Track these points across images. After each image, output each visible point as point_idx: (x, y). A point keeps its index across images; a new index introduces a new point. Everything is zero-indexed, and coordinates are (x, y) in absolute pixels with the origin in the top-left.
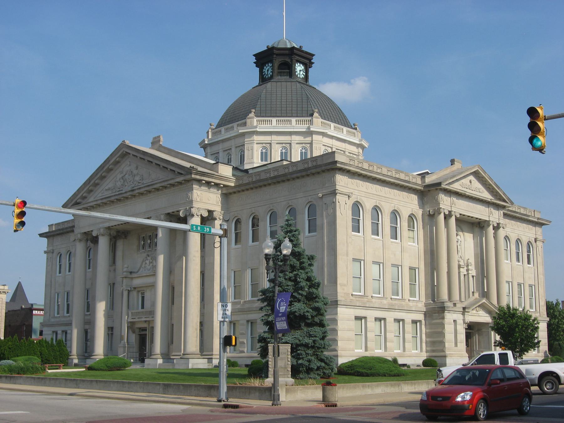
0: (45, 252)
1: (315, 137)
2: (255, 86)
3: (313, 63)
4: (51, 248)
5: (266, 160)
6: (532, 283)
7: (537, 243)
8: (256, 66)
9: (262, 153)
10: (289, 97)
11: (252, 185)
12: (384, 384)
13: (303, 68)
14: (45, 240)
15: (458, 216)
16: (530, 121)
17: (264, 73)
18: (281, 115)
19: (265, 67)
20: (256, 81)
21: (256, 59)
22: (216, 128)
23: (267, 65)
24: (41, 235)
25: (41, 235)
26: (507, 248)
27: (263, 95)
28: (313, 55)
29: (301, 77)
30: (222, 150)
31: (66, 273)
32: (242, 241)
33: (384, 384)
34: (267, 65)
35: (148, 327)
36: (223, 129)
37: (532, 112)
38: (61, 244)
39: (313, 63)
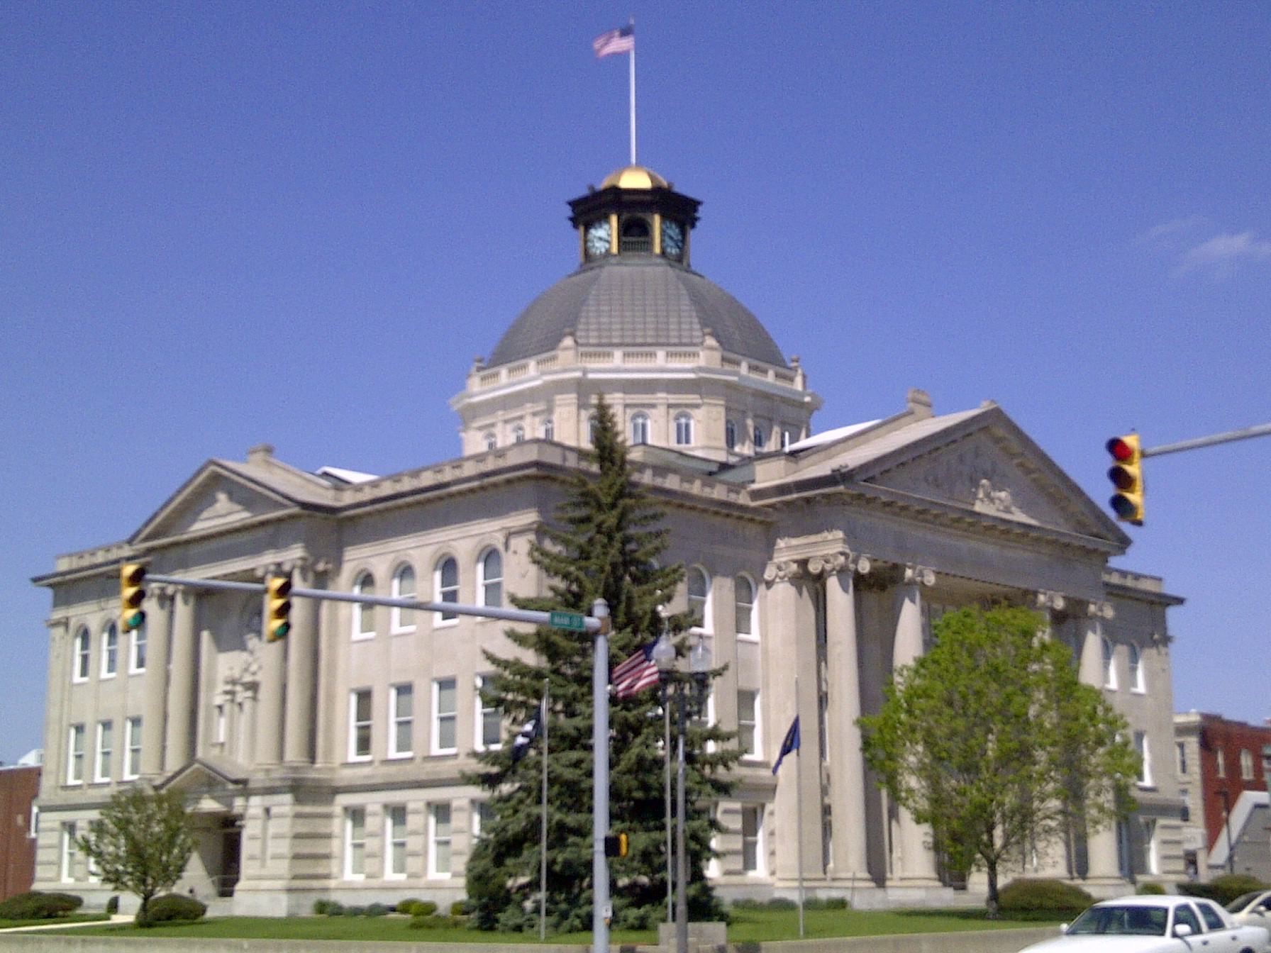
13: (677, 230)
25: (1180, 601)
28: (699, 203)
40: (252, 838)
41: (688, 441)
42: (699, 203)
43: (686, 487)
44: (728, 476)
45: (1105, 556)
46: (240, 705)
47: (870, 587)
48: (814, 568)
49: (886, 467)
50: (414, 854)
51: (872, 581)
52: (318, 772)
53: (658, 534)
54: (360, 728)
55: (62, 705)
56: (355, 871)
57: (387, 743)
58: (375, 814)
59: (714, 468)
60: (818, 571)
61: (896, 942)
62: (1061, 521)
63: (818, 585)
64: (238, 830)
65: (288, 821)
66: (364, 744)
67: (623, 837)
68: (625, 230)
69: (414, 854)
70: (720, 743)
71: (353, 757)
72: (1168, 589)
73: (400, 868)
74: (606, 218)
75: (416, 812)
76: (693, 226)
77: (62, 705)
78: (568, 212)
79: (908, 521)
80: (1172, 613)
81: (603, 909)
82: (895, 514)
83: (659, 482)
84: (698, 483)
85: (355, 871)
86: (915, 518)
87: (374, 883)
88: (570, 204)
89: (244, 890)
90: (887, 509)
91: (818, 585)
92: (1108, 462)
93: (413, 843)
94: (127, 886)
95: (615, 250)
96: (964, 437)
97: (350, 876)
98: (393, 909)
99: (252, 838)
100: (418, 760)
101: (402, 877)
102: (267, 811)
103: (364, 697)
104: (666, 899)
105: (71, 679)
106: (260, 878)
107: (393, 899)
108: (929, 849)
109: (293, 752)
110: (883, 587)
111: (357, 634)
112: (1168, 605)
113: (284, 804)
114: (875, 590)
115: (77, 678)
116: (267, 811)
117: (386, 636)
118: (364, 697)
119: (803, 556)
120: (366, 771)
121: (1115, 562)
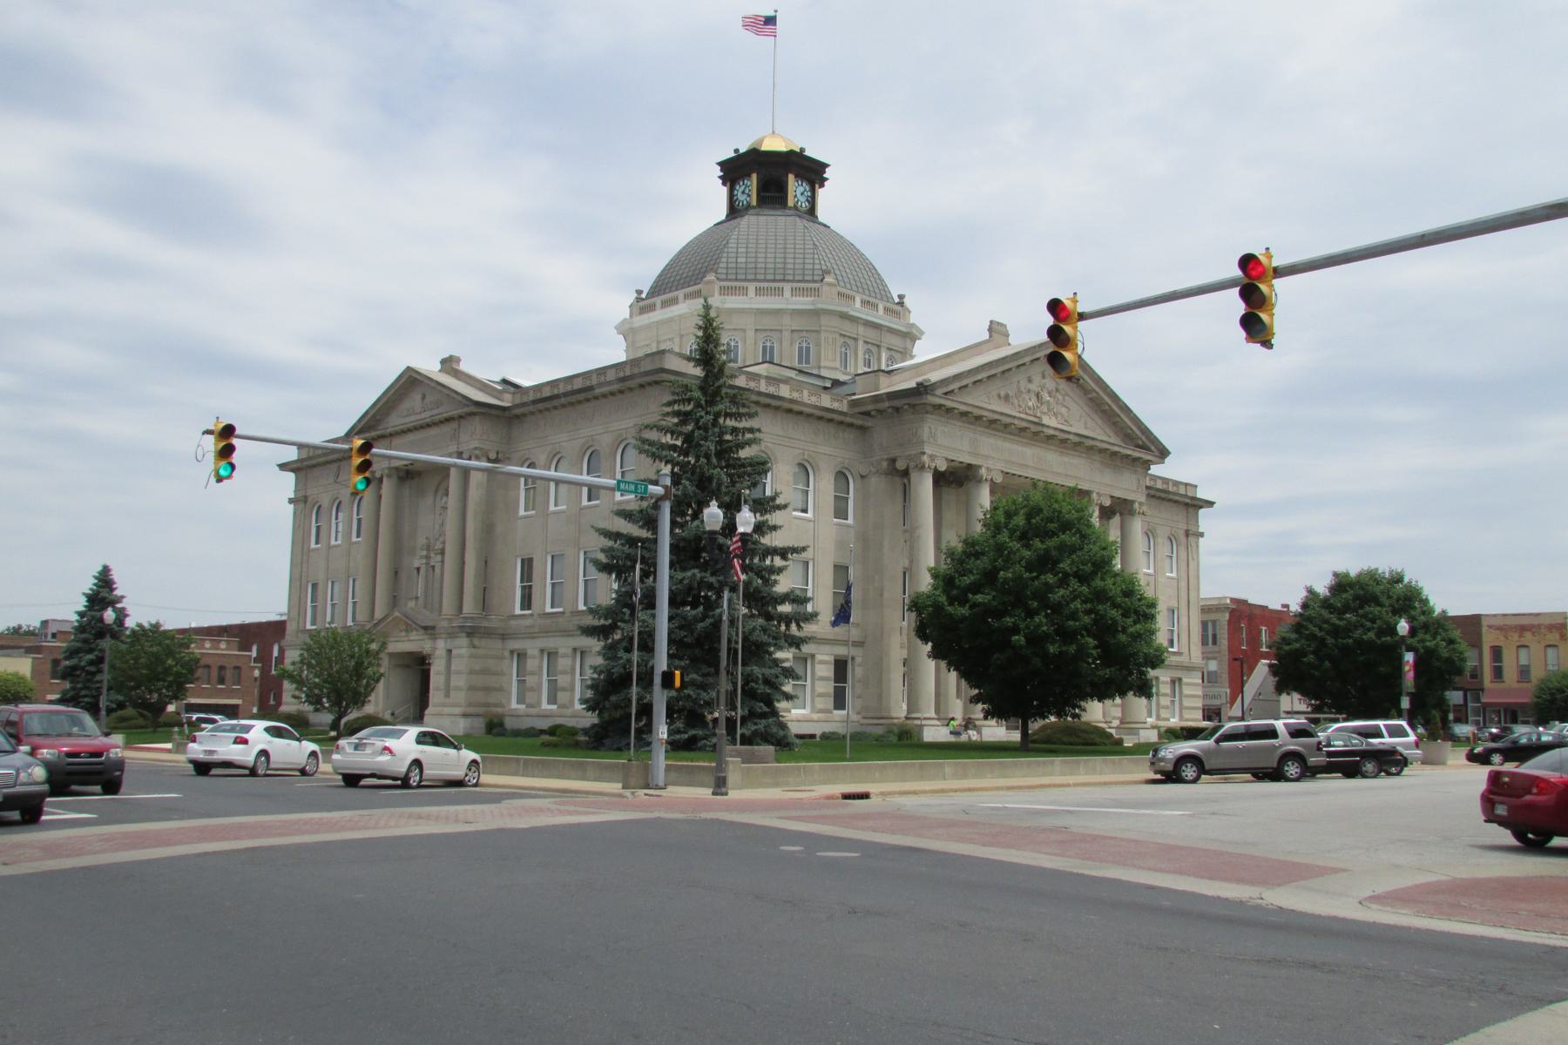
0: (291, 501)
1: (824, 320)
2: (719, 220)
3: (826, 179)
4: (302, 493)
5: (869, 367)
6: (1174, 604)
7: (1190, 539)
8: (724, 184)
9: (800, 349)
10: (771, 248)
11: (563, 399)
12: (896, 765)
14: (291, 476)
15: (999, 479)
16: (1244, 312)
17: (735, 198)
18: (801, 279)
19: (738, 187)
20: (721, 212)
21: (721, 171)
22: (646, 298)
23: (741, 183)
24: (1210, 504)
26: (1150, 549)
27: (732, 244)
28: (827, 166)
29: (804, 205)
30: (862, 338)
31: (351, 539)
32: (1564, 611)
33: (896, 765)
34: (741, 183)
35: (909, 742)
36: (658, 300)
37: (1055, 307)
38: (323, 490)
39: (826, 179)
40: (438, 673)
41: (808, 362)
42: (827, 166)
43: (795, 395)
44: (839, 390)
45: (1146, 464)
46: (433, 567)
47: (950, 483)
48: (901, 465)
49: (964, 383)
50: (532, 689)
51: (951, 479)
52: (494, 622)
53: (751, 430)
54: (523, 588)
55: (302, 567)
56: (549, 702)
57: (544, 602)
58: (534, 657)
59: (828, 384)
60: (904, 468)
61: (921, 765)
62: (1112, 434)
63: (906, 481)
64: (428, 667)
65: (1201, 700)
66: (527, 602)
67: (678, 673)
68: (763, 188)
69: (532, 689)
70: (795, 606)
71: (518, 611)
72: (1201, 494)
73: (552, 699)
74: (749, 176)
75: (565, 656)
76: (822, 186)
77: (302, 567)
78: (718, 172)
79: (982, 429)
80: (1202, 512)
81: (662, 731)
82: (970, 423)
83: (771, 390)
84: (806, 393)
85: (549, 702)
86: (987, 427)
87: (533, 711)
88: (719, 164)
89: (433, 715)
90: (964, 418)
91: (906, 481)
92: (1049, 320)
93: (562, 680)
94: (324, 708)
95: (754, 203)
96: (1032, 361)
97: (514, 705)
98: (542, 732)
99: (438, 673)
100: (568, 614)
101: (522, 707)
102: (450, 651)
103: (528, 565)
104: (1557, 723)
105: (309, 546)
106: (444, 705)
107: (544, 724)
108: (407, 666)
109: (469, 607)
110: (960, 484)
111: (522, 512)
112: (1201, 507)
113: (462, 646)
114: (953, 486)
115: (313, 545)
116: (450, 651)
117: (546, 514)
118: (528, 565)
119: (892, 456)
120: (528, 622)
121: (1155, 470)
